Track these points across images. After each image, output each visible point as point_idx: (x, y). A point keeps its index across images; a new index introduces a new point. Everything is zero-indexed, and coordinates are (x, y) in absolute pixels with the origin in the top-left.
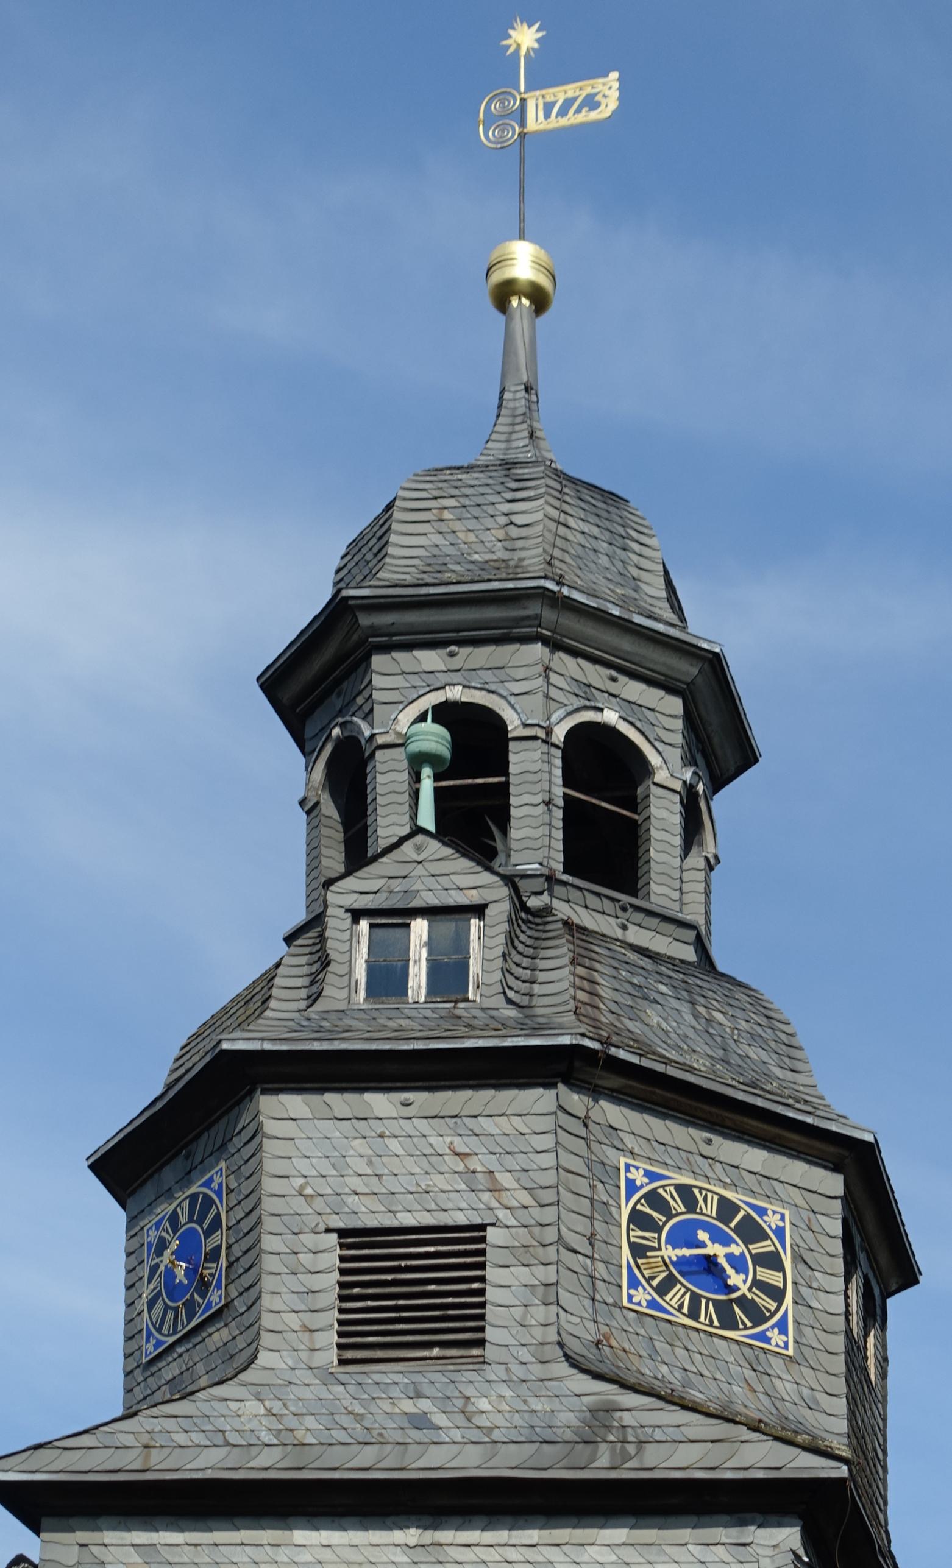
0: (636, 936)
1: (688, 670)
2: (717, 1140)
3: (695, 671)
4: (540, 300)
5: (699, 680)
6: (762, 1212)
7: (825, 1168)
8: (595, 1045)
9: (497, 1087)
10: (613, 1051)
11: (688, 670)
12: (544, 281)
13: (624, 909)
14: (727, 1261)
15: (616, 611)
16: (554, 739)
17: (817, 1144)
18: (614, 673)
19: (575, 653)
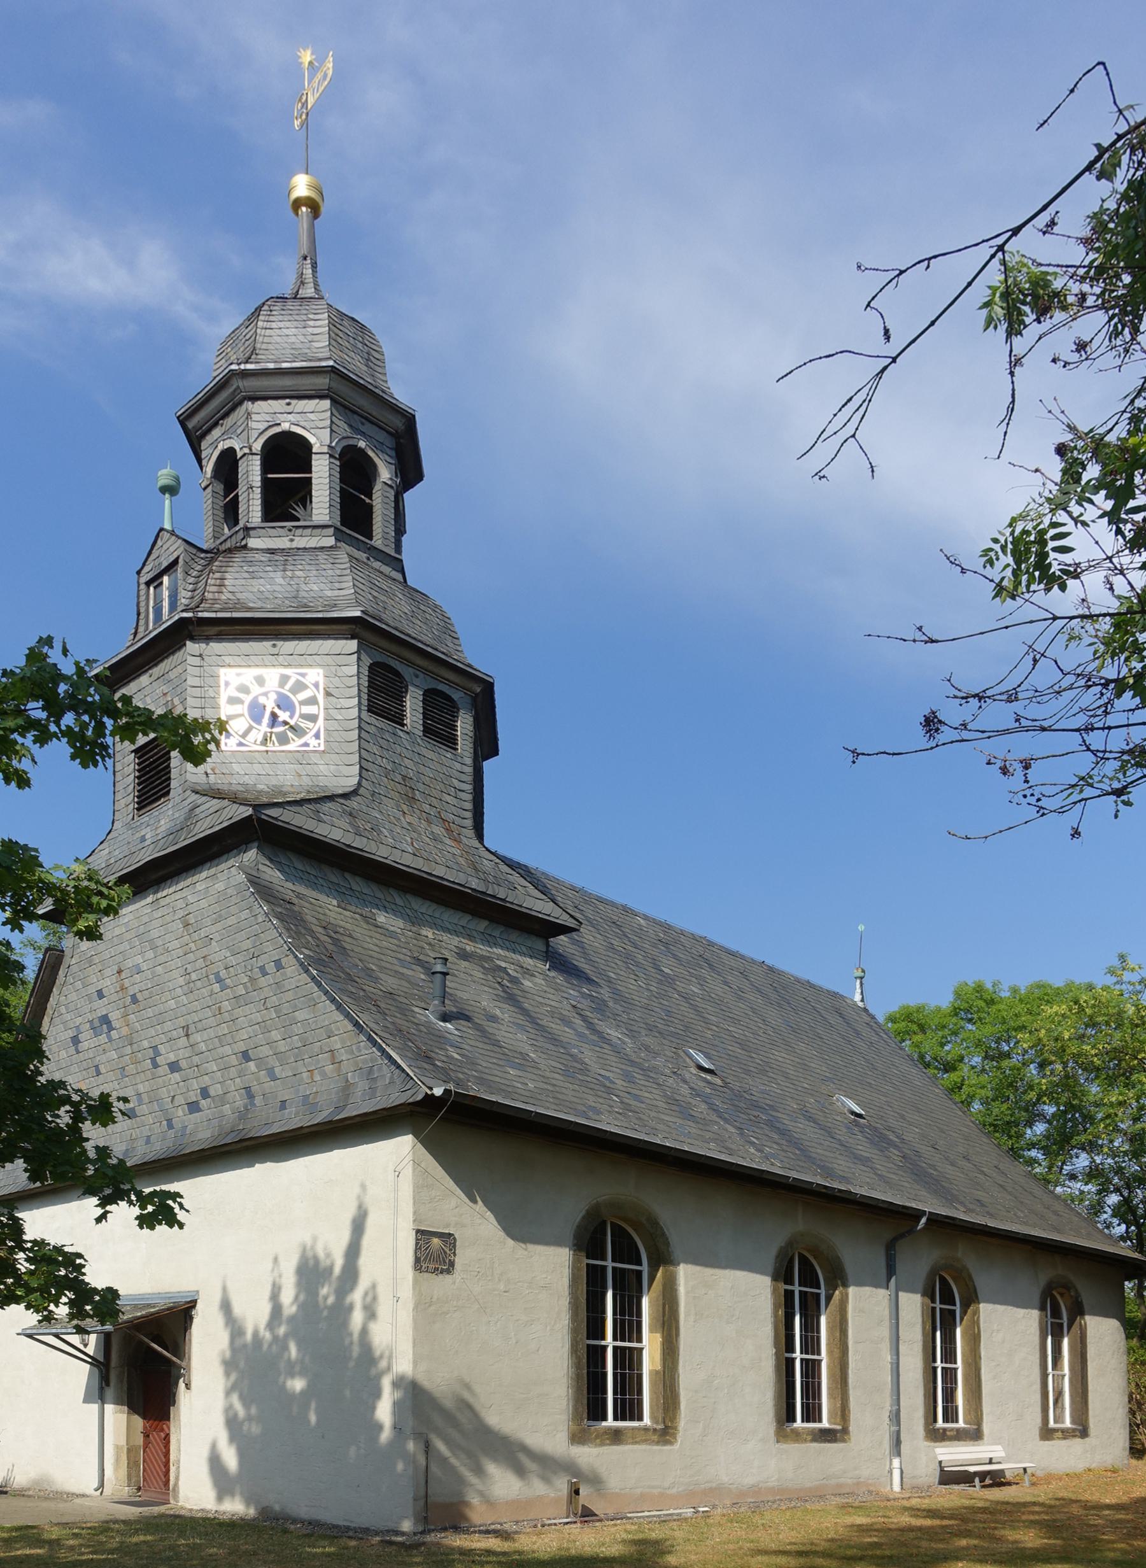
0: (300, 542)
1: (323, 382)
2: (279, 643)
3: (327, 380)
4: (314, 207)
5: (334, 385)
6: (303, 675)
7: (347, 639)
8: (190, 615)
9: (173, 653)
10: (200, 615)
11: (323, 382)
12: (313, 195)
13: (290, 530)
14: (449, 698)
15: (271, 366)
16: (254, 451)
17: (334, 627)
18: (288, 401)
19: (265, 398)
